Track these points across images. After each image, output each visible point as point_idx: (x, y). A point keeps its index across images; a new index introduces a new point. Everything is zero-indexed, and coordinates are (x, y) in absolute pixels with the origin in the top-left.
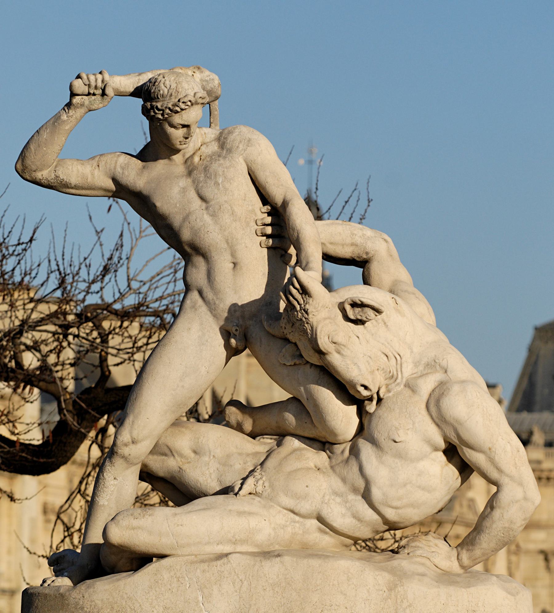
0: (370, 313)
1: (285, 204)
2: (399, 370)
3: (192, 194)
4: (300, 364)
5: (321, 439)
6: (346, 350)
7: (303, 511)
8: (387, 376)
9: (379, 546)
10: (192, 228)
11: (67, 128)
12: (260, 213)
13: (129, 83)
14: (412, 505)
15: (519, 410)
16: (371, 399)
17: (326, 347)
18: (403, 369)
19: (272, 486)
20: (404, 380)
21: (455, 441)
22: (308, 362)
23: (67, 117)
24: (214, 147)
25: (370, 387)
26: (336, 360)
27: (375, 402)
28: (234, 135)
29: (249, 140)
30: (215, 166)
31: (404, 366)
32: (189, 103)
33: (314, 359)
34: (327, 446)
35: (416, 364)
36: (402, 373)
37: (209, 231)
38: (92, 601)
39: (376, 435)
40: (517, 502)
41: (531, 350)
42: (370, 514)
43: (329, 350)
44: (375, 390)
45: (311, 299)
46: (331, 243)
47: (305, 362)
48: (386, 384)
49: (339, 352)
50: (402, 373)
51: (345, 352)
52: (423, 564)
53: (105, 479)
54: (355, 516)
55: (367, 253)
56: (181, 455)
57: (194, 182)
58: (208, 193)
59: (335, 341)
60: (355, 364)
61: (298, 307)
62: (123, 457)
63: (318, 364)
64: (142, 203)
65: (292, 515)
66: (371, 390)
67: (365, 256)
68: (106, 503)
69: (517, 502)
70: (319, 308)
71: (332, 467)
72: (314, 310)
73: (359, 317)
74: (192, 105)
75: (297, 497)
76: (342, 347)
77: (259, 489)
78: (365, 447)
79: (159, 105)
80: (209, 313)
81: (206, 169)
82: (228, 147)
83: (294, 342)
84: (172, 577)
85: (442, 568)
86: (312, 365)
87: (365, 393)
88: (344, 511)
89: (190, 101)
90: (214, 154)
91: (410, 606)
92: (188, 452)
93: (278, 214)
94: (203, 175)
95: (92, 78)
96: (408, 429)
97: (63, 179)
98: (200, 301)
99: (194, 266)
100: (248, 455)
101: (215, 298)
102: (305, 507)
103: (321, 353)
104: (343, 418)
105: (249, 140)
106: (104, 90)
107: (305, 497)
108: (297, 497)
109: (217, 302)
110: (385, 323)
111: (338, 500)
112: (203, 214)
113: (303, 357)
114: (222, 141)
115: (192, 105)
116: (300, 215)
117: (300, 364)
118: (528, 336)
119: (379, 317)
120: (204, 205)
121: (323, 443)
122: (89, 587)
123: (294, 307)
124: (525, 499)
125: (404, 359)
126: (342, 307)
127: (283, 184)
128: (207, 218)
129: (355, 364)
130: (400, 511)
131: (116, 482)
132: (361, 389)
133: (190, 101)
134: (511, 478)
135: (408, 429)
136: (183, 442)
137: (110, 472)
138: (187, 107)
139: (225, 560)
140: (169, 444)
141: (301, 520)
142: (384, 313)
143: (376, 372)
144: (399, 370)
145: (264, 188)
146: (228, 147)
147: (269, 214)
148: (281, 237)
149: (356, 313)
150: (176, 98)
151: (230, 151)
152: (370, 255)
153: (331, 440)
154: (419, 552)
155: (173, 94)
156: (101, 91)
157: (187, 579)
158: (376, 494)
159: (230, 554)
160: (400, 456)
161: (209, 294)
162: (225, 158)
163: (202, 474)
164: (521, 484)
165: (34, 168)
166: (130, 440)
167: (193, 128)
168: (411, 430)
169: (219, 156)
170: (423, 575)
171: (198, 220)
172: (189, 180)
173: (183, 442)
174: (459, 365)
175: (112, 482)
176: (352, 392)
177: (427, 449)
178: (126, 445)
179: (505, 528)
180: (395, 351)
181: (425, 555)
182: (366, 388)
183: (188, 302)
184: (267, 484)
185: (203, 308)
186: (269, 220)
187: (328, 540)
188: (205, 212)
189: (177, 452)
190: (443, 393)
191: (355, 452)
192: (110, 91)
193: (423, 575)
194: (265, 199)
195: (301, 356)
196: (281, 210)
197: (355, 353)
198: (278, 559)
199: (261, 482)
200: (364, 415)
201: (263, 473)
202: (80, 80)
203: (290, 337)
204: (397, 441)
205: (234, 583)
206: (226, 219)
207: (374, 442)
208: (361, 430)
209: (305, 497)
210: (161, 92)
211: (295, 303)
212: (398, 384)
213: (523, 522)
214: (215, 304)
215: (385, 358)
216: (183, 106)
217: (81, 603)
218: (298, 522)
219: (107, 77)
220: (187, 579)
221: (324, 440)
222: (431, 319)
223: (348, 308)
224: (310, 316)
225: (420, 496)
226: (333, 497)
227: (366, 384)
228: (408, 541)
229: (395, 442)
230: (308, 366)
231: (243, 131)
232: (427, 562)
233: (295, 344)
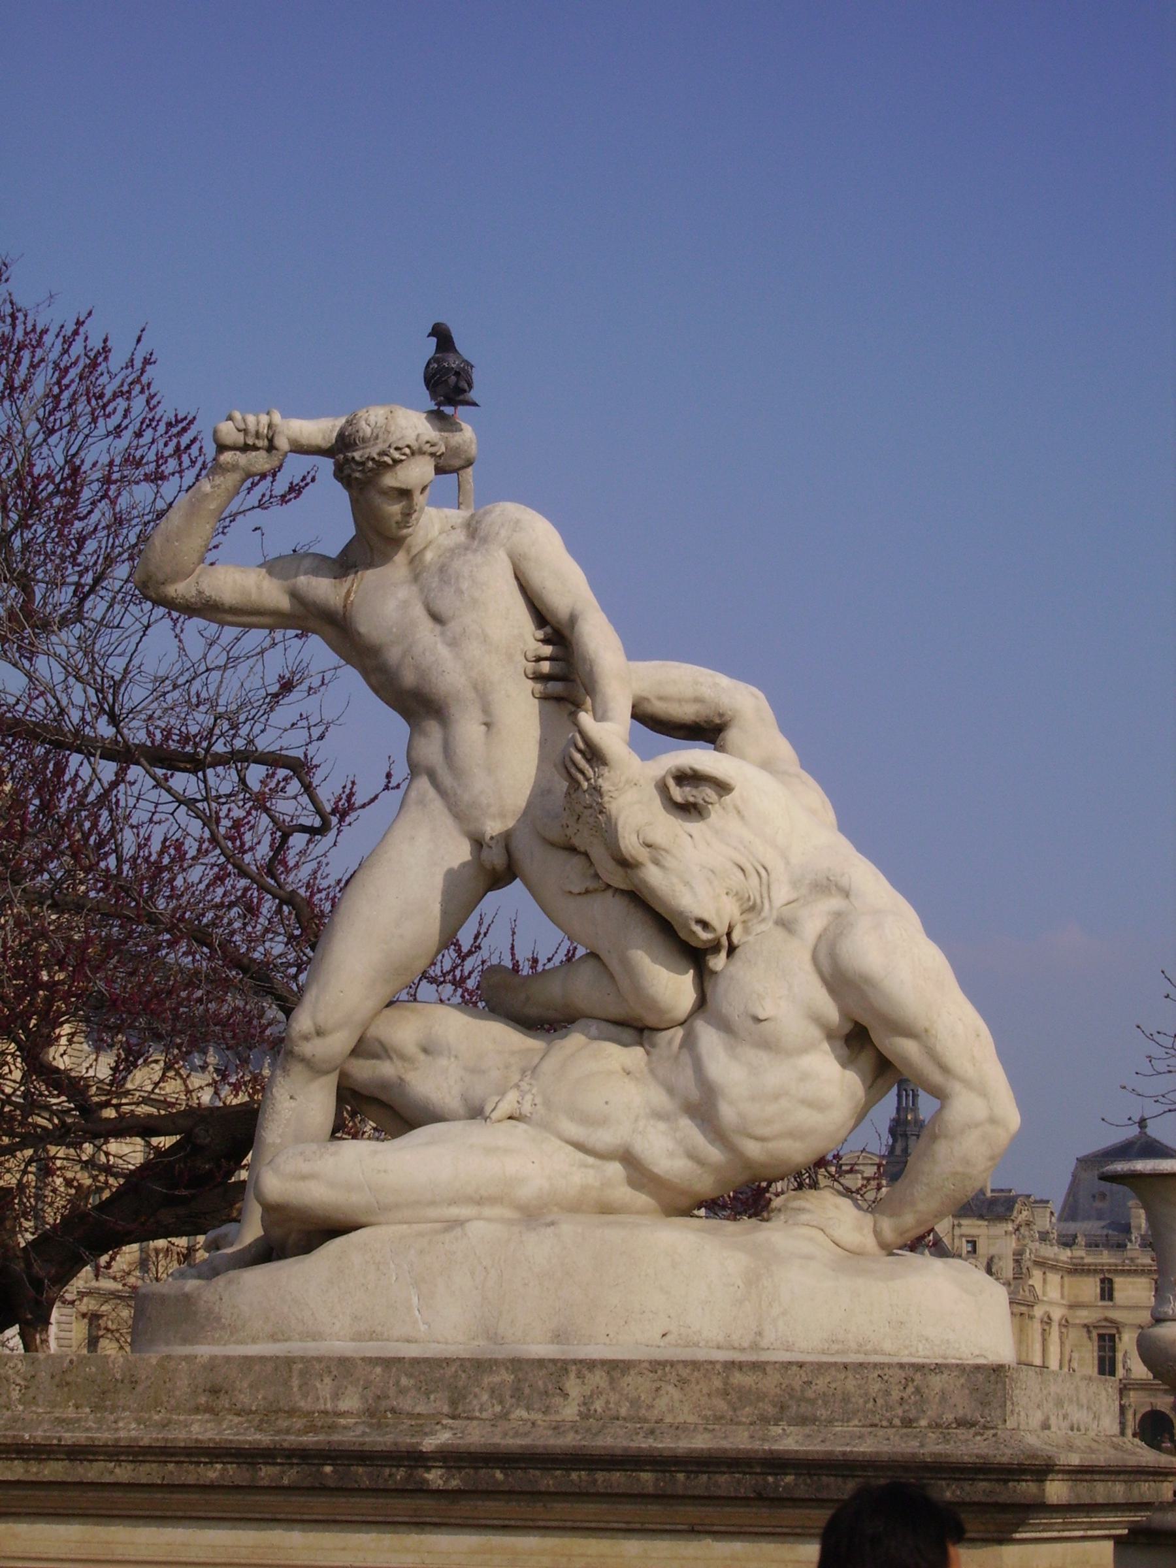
0: (709, 793)
1: (573, 620)
2: (765, 895)
3: (418, 612)
4: (595, 890)
5: (635, 1024)
6: (669, 858)
7: (600, 1146)
8: (746, 906)
9: (132, 852)
10: (417, 667)
11: (212, 507)
12: (527, 637)
13: (318, 429)
14: (792, 1134)
15: (1066, 1220)
16: (715, 948)
17: (633, 852)
18: (772, 894)
19: (547, 1103)
20: (775, 913)
21: (865, 1020)
22: (609, 886)
23: (212, 487)
24: (460, 537)
25: (715, 922)
26: (653, 876)
27: (723, 954)
28: (493, 515)
29: (518, 522)
30: (457, 564)
31: (774, 888)
32: (407, 451)
33: (617, 878)
34: (646, 1033)
35: (795, 884)
36: (770, 901)
37: (442, 663)
38: (234, 1307)
39: (726, 1009)
40: (977, 1126)
41: (1074, 1176)
42: (714, 1154)
43: (640, 859)
44: (722, 929)
45: (606, 769)
46: (660, 698)
47: (603, 886)
48: (744, 922)
49: (656, 862)
50: (770, 901)
51: (669, 862)
52: (811, 1239)
53: (274, 1098)
54: (692, 1155)
55: (721, 715)
56: (403, 1057)
57: (421, 590)
58: (444, 605)
59: (649, 840)
60: (687, 883)
61: (585, 785)
62: (303, 1060)
63: (623, 886)
64: (338, 628)
65: (580, 1156)
66: (714, 930)
67: (718, 721)
68: (278, 1141)
69: (977, 1126)
70: (621, 785)
71: (652, 1071)
72: (611, 788)
73: (691, 799)
74: (413, 453)
75: (586, 1119)
76: (663, 853)
77: (527, 1108)
78: (708, 1037)
79: (357, 455)
80: (446, 811)
81: (442, 569)
82: (482, 534)
83: (582, 849)
84: (367, 1262)
85: (847, 1247)
86: (616, 890)
87: (705, 936)
88: (671, 1145)
89: (408, 446)
90: (458, 546)
91: (784, 1313)
92: (411, 1048)
93: (558, 633)
94: (436, 579)
95: (251, 419)
96: (780, 998)
97: (210, 597)
98: (432, 793)
99: (423, 733)
100: (513, 1053)
101: (455, 785)
102: (605, 1138)
103: (626, 864)
104: (673, 987)
105: (518, 522)
106: (271, 440)
107: (602, 1121)
108: (586, 1119)
109: (459, 792)
110: (739, 812)
111: (662, 1126)
112: (436, 643)
113: (599, 878)
114: (472, 529)
115: (413, 453)
116: (600, 640)
117: (595, 890)
118: (1072, 1165)
119: (727, 799)
120: (438, 628)
121: (637, 1028)
122: (230, 1282)
123: (579, 785)
124: (993, 1120)
125: (773, 876)
126: (663, 788)
127: (569, 585)
128: (443, 651)
129: (687, 883)
130: (770, 1145)
131: (293, 1104)
132: (698, 929)
133: (408, 446)
134: (967, 1083)
135: (780, 998)
136: (404, 1031)
137: (283, 1087)
138: (403, 457)
139: (458, 1232)
140: (382, 1038)
141: (598, 1162)
142: (735, 794)
143: (725, 897)
144: (765, 895)
145: (540, 598)
146: (482, 534)
147: (546, 641)
148: (564, 678)
149: (689, 797)
150: (384, 441)
151: (485, 540)
152: (727, 718)
153: (651, 1020)
154: (804, 1217)
155: (381, 435)
156: (266, 442)
157: (392, 1266)
158: (727, 1113)
159: (468, 1221)
160: (768, 1045)
161: (447, 780)
162: (476, 551)
163: (431, 1083)
164: (983, 1093)
165: (161, 577)
166: (312, 1030)
167: (419, 499)
168: (779, 986)
169: (466, 549)
170: (809, 1257)
171: (427, 654)
172: (415, 588)
173: (404, 1031)
174: (867, 880)
175: (287, 1104)
176: (682, 935)
177: (815, 1033)
178: (306, 1038)
179: (957, 1173)
180: (758, 861)
181: (815, 1223)
182: (705, 925)
183: (413, 794)
184: (538, 1100)
185: (437, 804)
186: (548, 650)
187: (642, 1199)
188: (438, 639)
189: (395, 1051)
190: (842, 933)
191: (689, 1042)
192: (282, 443)
193: (809, 1257)
194: (540, 616)
195: (596, 876)
196: (566, 632)
197: (695, 871)
198: (550, 1230)
199: (529, 1097)
200: (707, 978)
201: (533, 1082)
202: (230, 422)
203: (576, 841)
204: (761, 1017)
205: (472, 1273)
206: (474, 650)
207: (725, 1026)
208: (702, 1002)
209: (602, 1121)
210: (361, 434)
211: (580, 777)
212: (763, 920)
213: (989, 1164)
214: (455, 794)
215: (740, 874)
216: (397, 455)
217: (217, 1310)
218: (592, 1166)
219: (277, 418)
220: (392, 1266)
221: (640, 1025)
222: (831, 816)
223: (671, 783)
224: (606, 799)
225: (805, 1117)
226: (652, 1122)
227: (706, 916)
228: (787, 1200)
229: (760, 1021)
230: (610, 893)
231: (511, 510)
232: (819, 1235)
233: (586, 855)
